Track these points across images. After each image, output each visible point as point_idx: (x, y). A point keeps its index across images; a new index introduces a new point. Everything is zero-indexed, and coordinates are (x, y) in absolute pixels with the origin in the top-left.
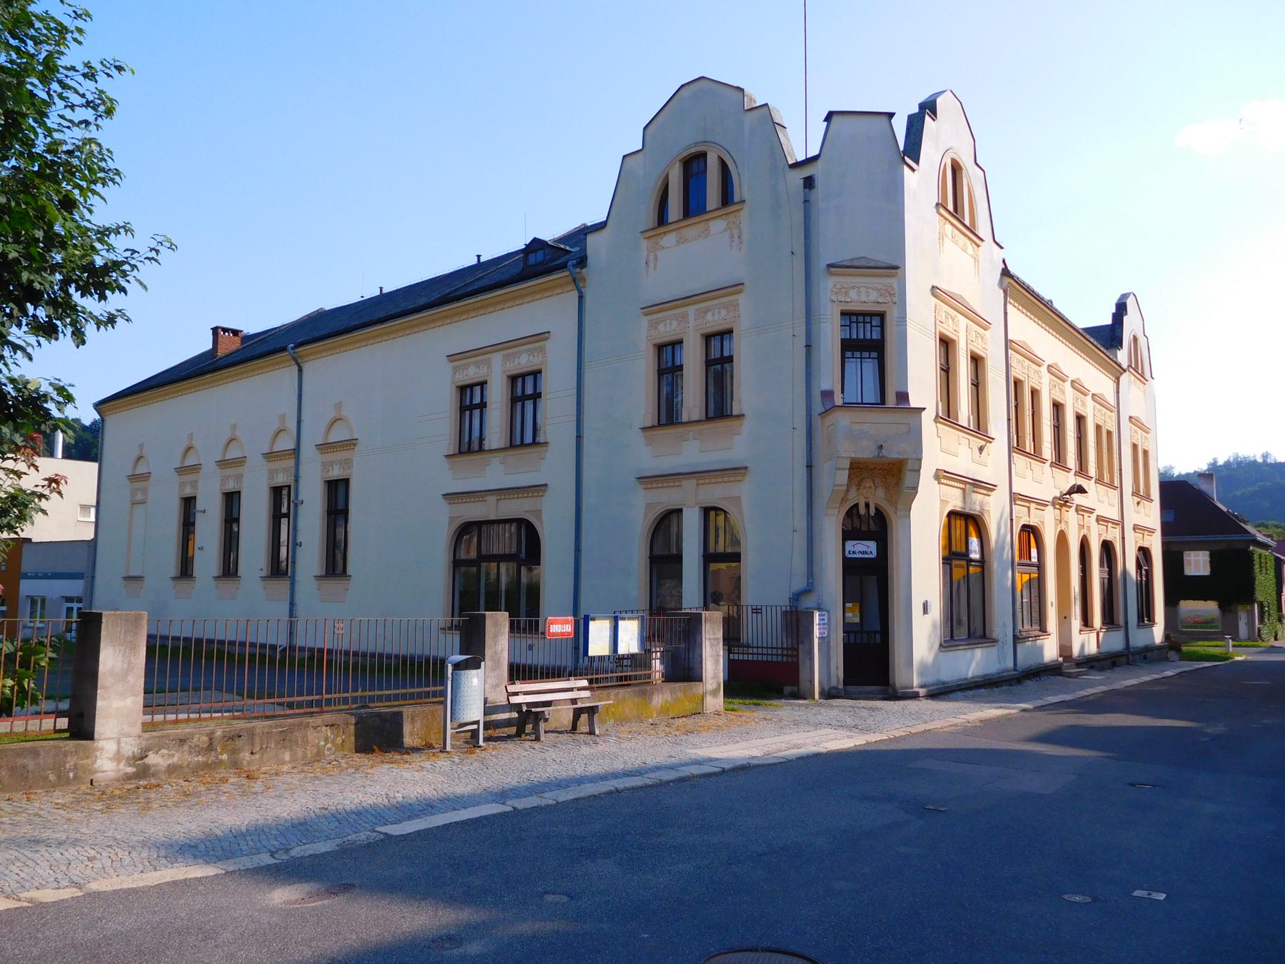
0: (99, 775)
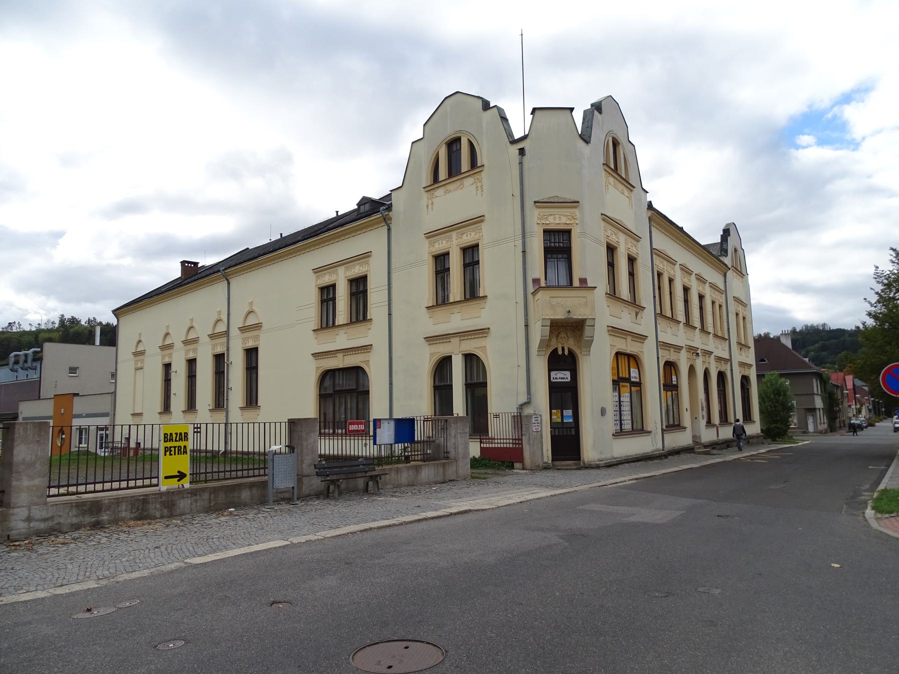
0: (14, 532)
